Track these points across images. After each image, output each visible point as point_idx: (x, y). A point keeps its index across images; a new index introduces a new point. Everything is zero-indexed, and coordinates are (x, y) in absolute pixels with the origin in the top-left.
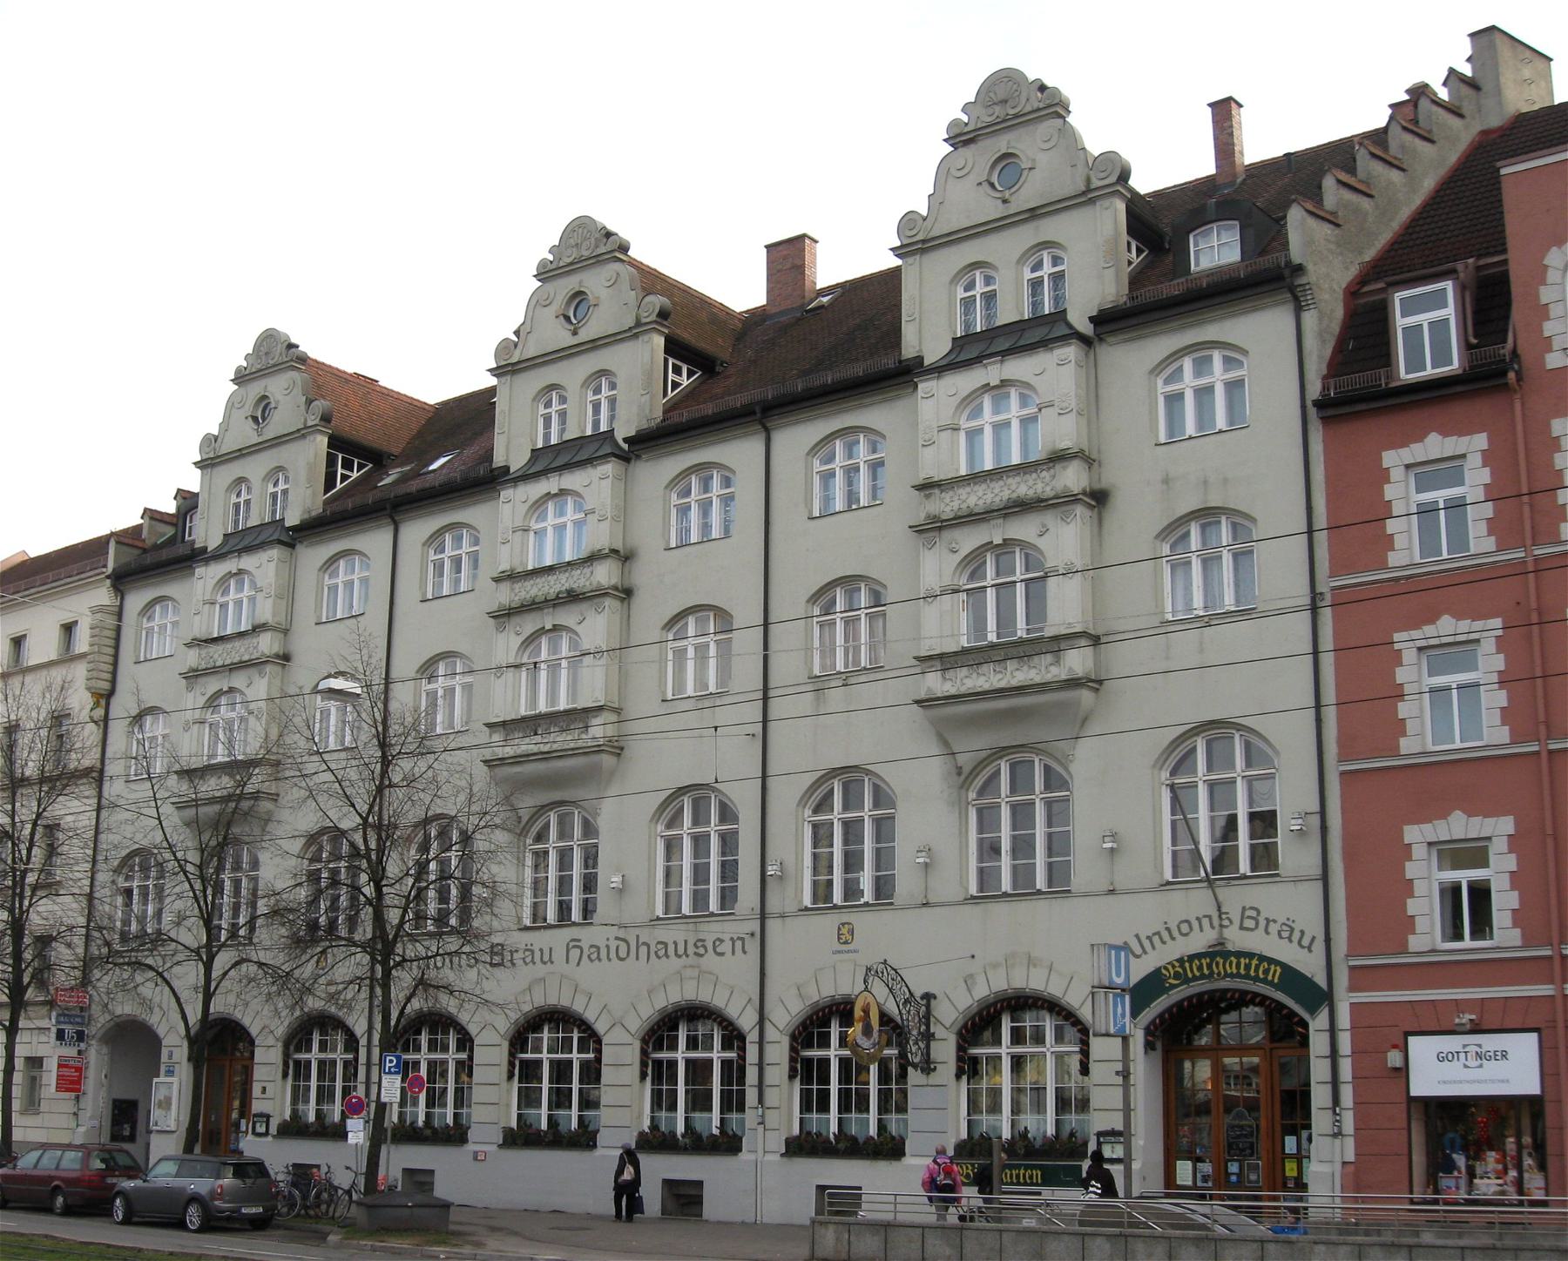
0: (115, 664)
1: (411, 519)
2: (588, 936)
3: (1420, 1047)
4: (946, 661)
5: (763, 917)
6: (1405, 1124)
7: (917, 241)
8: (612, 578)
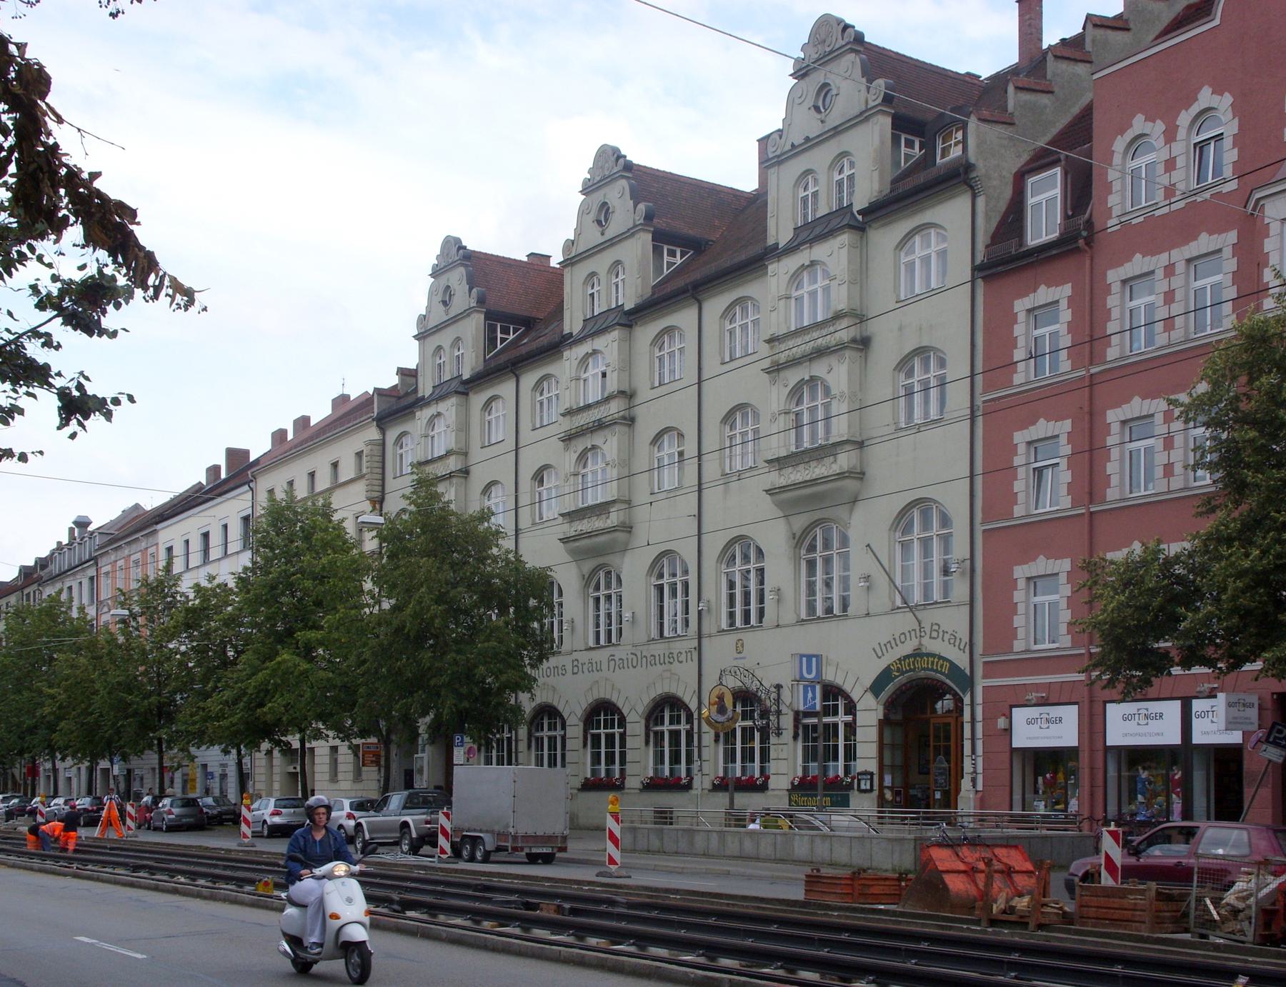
0: (383, 480)
1: (711, 297)
2: (620, 653)
3: (1019, 715)
4: (780, 463)
5: (700, 637)
6: (1008, 766)
7: (773, 153)
8: (622, 409)
